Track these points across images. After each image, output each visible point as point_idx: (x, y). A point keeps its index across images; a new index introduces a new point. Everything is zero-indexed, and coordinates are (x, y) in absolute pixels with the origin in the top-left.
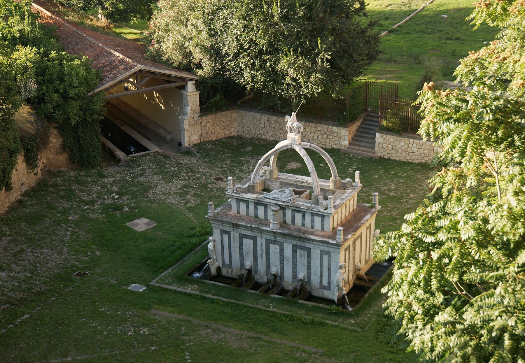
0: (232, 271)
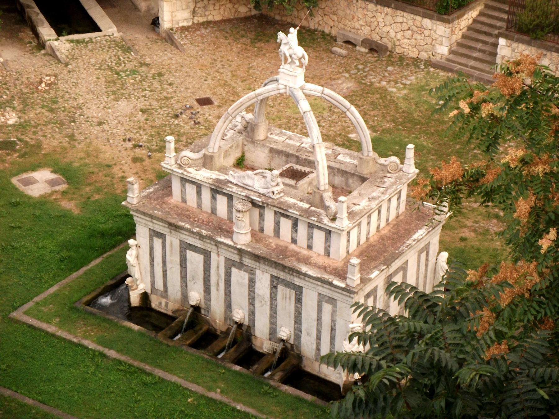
0: (167, 304)
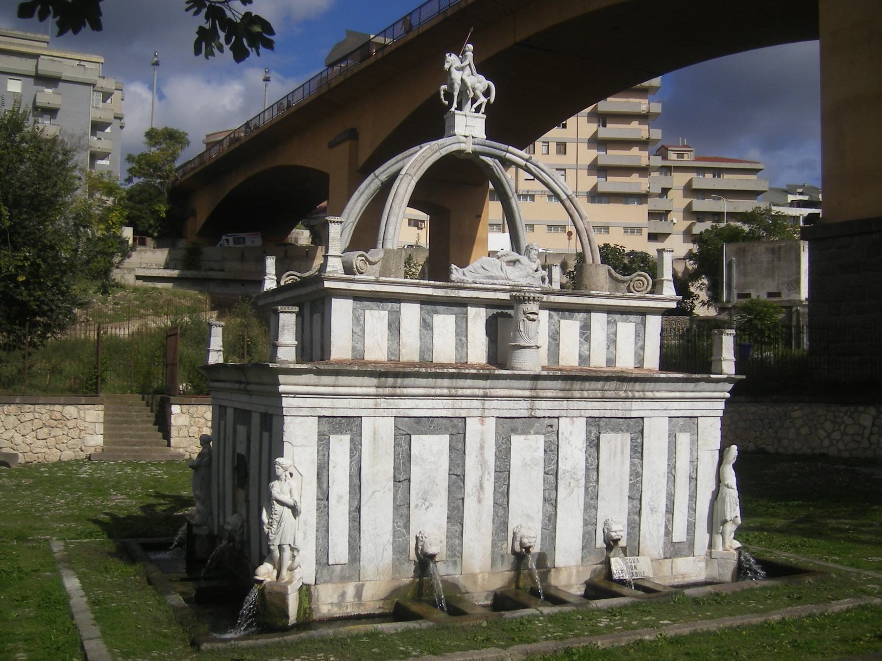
0: (359, 594)
